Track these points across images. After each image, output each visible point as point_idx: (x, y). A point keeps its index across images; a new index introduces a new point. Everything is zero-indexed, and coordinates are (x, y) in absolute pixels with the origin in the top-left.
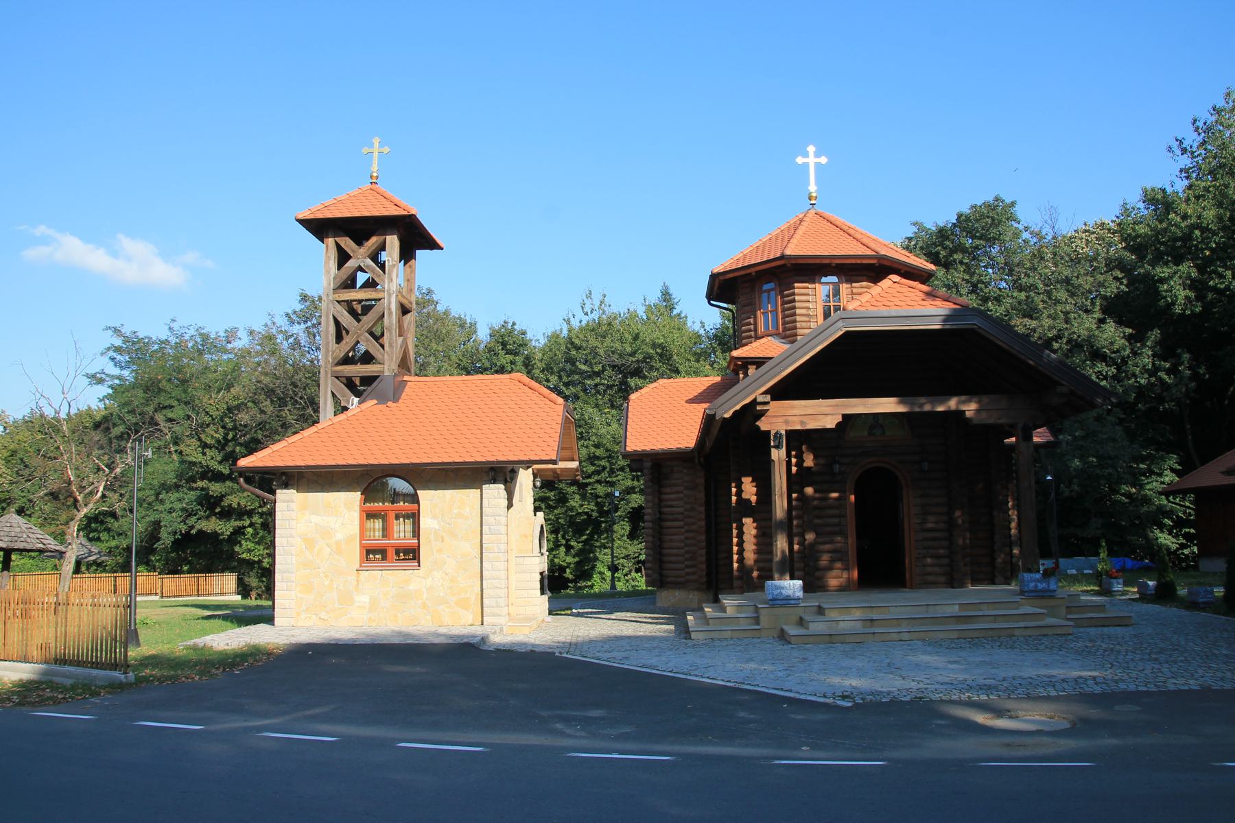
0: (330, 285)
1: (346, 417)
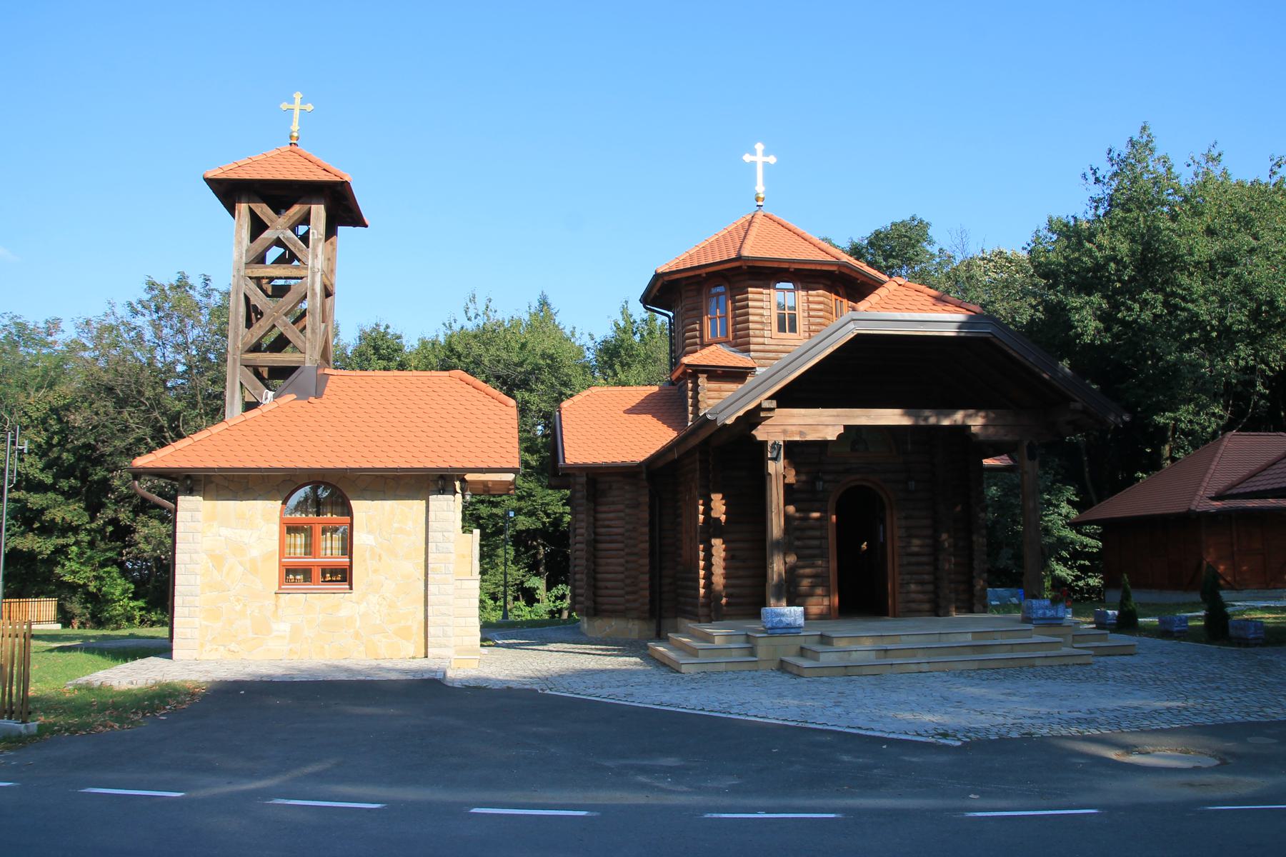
0: (241, 257)
1: (261, 413)
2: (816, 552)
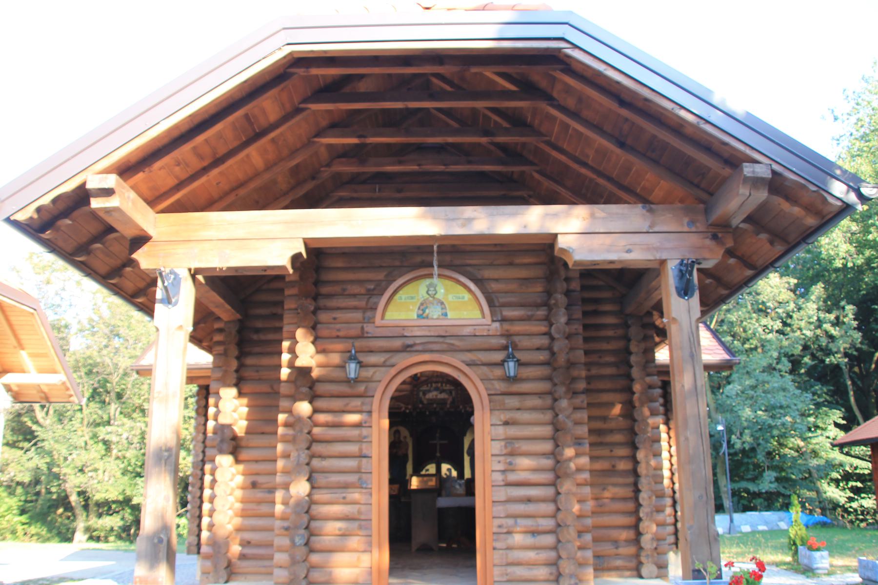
2: (352, 478)
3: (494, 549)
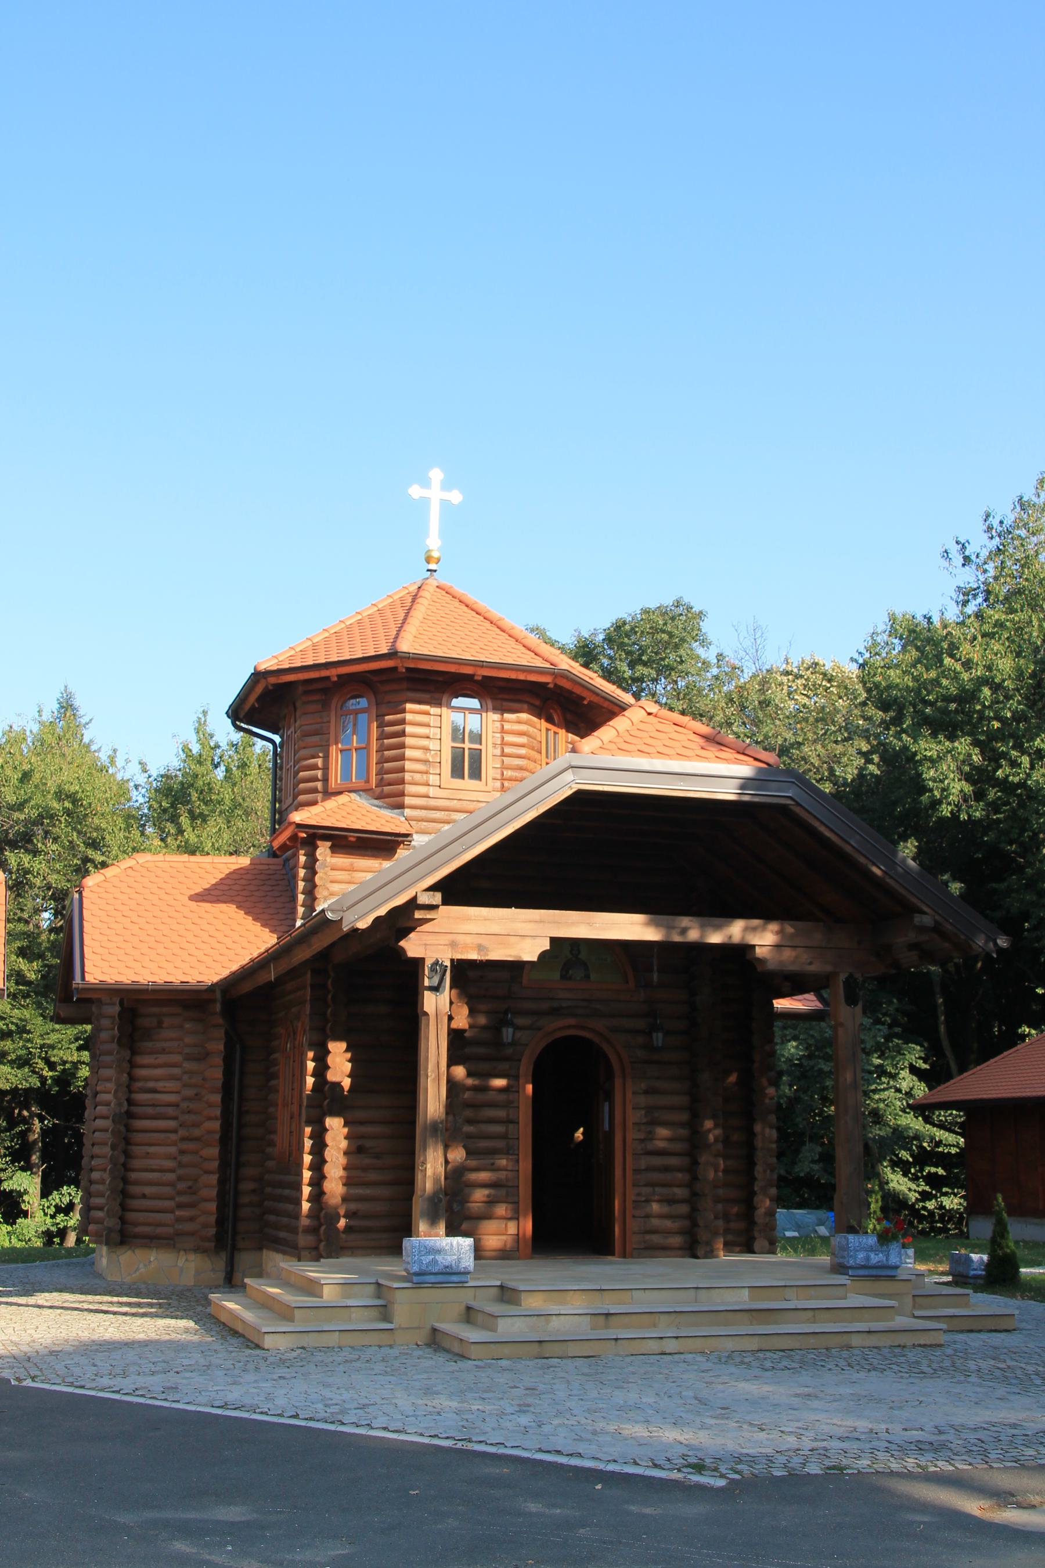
2: (500, 1144)
3: (634, 1216)
